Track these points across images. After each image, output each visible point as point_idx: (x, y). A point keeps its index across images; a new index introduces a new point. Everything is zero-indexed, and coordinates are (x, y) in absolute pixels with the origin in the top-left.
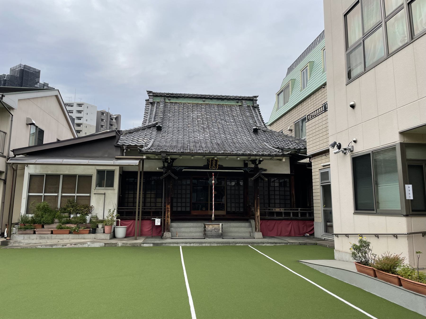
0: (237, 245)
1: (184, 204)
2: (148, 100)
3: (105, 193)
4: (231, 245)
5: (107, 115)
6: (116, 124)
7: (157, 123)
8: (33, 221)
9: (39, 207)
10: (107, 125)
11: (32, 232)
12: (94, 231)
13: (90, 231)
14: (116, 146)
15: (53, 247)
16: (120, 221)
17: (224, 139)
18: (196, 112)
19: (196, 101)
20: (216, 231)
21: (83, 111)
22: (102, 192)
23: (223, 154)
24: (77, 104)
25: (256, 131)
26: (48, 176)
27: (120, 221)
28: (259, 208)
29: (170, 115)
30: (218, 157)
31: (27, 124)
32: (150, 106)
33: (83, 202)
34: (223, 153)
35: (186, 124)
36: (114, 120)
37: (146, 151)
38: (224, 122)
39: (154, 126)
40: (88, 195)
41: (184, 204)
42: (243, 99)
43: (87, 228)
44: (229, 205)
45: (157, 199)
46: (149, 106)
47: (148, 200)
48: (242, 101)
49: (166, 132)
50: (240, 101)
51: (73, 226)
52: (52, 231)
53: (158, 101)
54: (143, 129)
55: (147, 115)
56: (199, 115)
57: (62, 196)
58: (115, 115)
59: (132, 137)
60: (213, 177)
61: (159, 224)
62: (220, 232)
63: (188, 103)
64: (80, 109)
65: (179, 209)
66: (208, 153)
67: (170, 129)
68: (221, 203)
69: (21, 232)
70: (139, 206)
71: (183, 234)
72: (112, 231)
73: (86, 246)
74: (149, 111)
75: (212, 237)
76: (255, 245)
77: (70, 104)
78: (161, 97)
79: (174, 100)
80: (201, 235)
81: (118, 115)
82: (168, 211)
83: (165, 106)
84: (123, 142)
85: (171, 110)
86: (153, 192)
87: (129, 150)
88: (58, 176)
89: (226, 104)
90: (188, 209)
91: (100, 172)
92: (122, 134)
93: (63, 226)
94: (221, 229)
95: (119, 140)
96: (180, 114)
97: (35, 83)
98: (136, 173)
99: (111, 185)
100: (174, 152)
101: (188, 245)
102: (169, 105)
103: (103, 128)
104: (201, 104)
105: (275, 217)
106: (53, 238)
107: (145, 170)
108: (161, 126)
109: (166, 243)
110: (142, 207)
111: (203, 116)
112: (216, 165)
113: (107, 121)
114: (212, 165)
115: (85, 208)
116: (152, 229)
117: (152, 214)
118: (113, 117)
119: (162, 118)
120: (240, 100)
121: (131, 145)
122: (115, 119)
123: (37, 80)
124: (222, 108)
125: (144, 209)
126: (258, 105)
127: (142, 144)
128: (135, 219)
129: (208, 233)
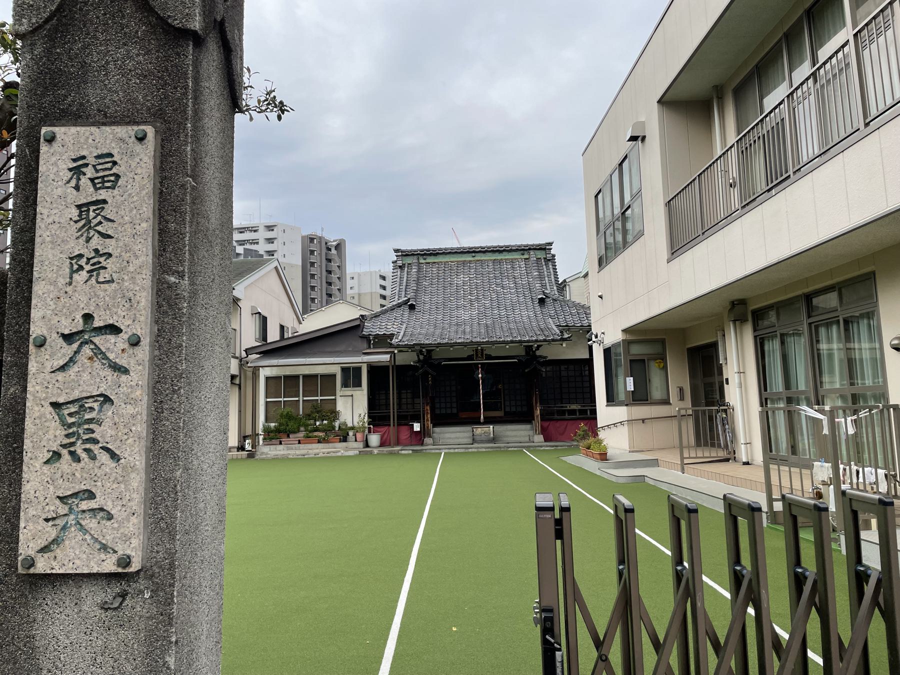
0: (510, 449)
1: (449, 405)
2: (396, 262)
4: (502, 449)
5: (320, 242)
6: (337, 258)
7: (409, 300)
8: (277, 431)
9: (282, 414)
11: (278, 442)
12: (345, 439)
13: (340, 439)
15: (305, 457)
17: (497, 317)
18: (462, 276)
21: (276, 238)
22: (349, 393)
23: (487, 343)
24: (266, 226)
25: (542, 301)
26: (286, 377)
28: (538, 405)
29: (427, 284)
30: (482, 346)
31: (252, 314)
32: (399, 270)
33: (328, 407)
34: (488, 341)
35: (447, 296)
36: (334, 251)
37: (397, 345)
38: (500, 289)
39: (405, 303)
40: (333, 397)
41: (449, 405)
42: (530, 249)
43: (337, 436)
44: (507, 403)
45: (415, 400)
47: (404, 401)
50: (526, 252)
51: (321, 434)
52: (299, 441)
55: (396, 285)
56: (466, 279)
57: (303, 400)
58: (334, 241)
59: (379, 323)
61: (419, 429)
62: (492, 436)
63: (451, 262)
64: (270, 235)
65: (443, 411)
66: (470, 342)
67: (427, 307)
68: (864, 410)
69: (266, 443)
70: (393, 409)
71: (448, 441)
72: (365, 439)
73: (339, 454)
74: (398, 280)
75: (482, 442)
76: (532, 448)
77: (252, 227)
78: (412, 257)
79: (430, 259)
80: (470, 441)
82: (427, 413)
83: (419, 270)
84: (369, 330)
85: (427, 275)
86: (409, 391)
87: (377, 340)
89: (506, 258)
90: (455, 411)
94: (492, 433)
95: (363, 328)
96: (432, 310)
98: (388, 366)
99: (358, 384)
100: (429, 344)
101: (452, 451)
104: (470, 262)
105: (567, 416)
106: (301, 448)
107: (397, 364)
108: (414, 303)
109: (426, 450)
111: (472, 282)
113: (320, 254)
114: (477, 355)
115: (331, 414)
117: (409, 418)
119: (415, 291)
120: (526, 250)
121: (379, 335)
122: (335, 249)
124: (499, 266)
125: (400, 412)
126: (554, 256)
127: (391, 332)
128: (390, 425)
129: (477, 438)
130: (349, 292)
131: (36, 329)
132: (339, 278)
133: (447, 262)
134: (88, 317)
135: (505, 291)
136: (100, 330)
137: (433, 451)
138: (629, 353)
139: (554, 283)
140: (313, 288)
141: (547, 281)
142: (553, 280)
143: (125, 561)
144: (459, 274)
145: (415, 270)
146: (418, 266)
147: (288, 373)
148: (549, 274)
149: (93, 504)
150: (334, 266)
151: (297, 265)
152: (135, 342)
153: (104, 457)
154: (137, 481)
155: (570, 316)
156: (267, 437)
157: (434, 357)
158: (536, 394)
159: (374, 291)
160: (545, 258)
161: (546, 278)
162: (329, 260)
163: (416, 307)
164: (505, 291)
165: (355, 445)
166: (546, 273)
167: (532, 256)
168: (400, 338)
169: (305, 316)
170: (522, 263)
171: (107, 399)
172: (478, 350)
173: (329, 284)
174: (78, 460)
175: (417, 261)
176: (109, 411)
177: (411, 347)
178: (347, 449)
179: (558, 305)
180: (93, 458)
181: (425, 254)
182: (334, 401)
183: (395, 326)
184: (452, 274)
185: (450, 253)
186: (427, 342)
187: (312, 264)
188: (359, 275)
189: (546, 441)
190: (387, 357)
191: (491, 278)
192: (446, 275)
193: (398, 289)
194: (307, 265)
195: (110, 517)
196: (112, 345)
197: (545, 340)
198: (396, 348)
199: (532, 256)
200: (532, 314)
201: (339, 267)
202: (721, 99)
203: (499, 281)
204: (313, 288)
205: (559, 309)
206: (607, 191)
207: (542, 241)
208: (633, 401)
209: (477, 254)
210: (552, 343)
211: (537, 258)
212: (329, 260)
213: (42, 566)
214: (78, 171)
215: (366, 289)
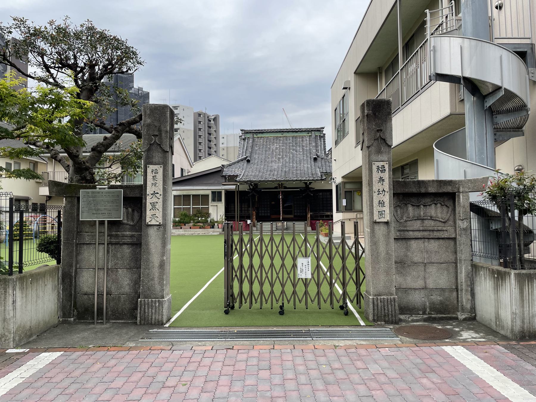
5: (204, 116)
6: (214, 126)
7: (247, 157)
8: (180, 222)
9: (182, 214)
10: (205, 128)
11: (180, 228)
12: (213, 227)
14: (222, 176)
18: (276, 144)
22: (216, 204)
25: (315, 159)
26: (184, 196)
28: (309, 212)
33: (205, 211)
34: (284, 180)
36: (212, 122)
39: (245, 159)
40: (208, 206)
44: (296, 211)
50: (310, 132)
51: (201, 224)
52: (190, 227)
54: (238, 162)
56: (278, 146)
58: (213, 116)
62: (286, 227)
65: (263, 214)
66: (275, 180)
69: (174, 228)
74: (242, 146)
79: (259, 135)
81: (216, 115)
85: (257, 144)
88: (190, 195)
89: (300, 135)
90: (269, 214)
91: (213, 193)
93: (196, 224)
97: (130, 89)
98: (235, 191)
100: (255, 181)
104: (280, 137)
105: (325, 218)
106: (191, 231)
107: (240, 190)
112: (282, 186)
113: (204, 123)
116: (246, 227)
123: (131, 84)
125: (241, 214)
126: (324, 134)
127: (237, 174)
128: (235, 221)
130: (221, 146)
131: (148, 193)
132: (215, 138)
133: (268, 137)
134: (154, 192)
135: (297, 153)
136: (156, 193)
137: (256, 234)
139: (323, 149)
140: (200, 143)
142: (323, 148)
143: (160, 223)
144: (274, 144)
146: (253, 139)
147: (185, 194)
148: (321, 144)
149: (156, 216)
150: (212, 130)
151: (191, 130)
152: (161, 195)
153: (157, 210)
154: (161, 213)
156: (174, 225)
157: (259, 187)
159: (235, 146)
160: (320, 136)
161: (319, 147)
162: (210, 127)
164: (297, 153)
165: (218, 230)
166: (319, 144)
167: (313, 134)
168: (241, 177)
169: (194, 163)
171: (157, 202)
172: (280, 184)
175: (252, 136)
176: (157, 204)
177: (246, 182)
178: (214, 232)
179: (323, 161)
180: (155, 210)
181: (257, 133)
182: (208, 208)
183: (239, 171)
184: (271, 144)
185: (270, 132)
186: (254, 180)
187: (200, 129)
188: (227, 136)
189: (312, 230)
190: (234, 187)
191: (290, 146)
192: (267, 144)
194: (197, 130)
195: (158, 218)
197: (313, 180)
198: (238, 182)
199: (313, 134)
200: (309, 166)
201: (215, 131)
202: (381, 73)
204: (200, 143)
205: (323, 163)
206: (338, 109)
207: (319, 126)
209: (284, 133)
211: (315, 136)
212: (210, 127)
213: (149, 223)
214: (152, 171)
215: (231, 145)
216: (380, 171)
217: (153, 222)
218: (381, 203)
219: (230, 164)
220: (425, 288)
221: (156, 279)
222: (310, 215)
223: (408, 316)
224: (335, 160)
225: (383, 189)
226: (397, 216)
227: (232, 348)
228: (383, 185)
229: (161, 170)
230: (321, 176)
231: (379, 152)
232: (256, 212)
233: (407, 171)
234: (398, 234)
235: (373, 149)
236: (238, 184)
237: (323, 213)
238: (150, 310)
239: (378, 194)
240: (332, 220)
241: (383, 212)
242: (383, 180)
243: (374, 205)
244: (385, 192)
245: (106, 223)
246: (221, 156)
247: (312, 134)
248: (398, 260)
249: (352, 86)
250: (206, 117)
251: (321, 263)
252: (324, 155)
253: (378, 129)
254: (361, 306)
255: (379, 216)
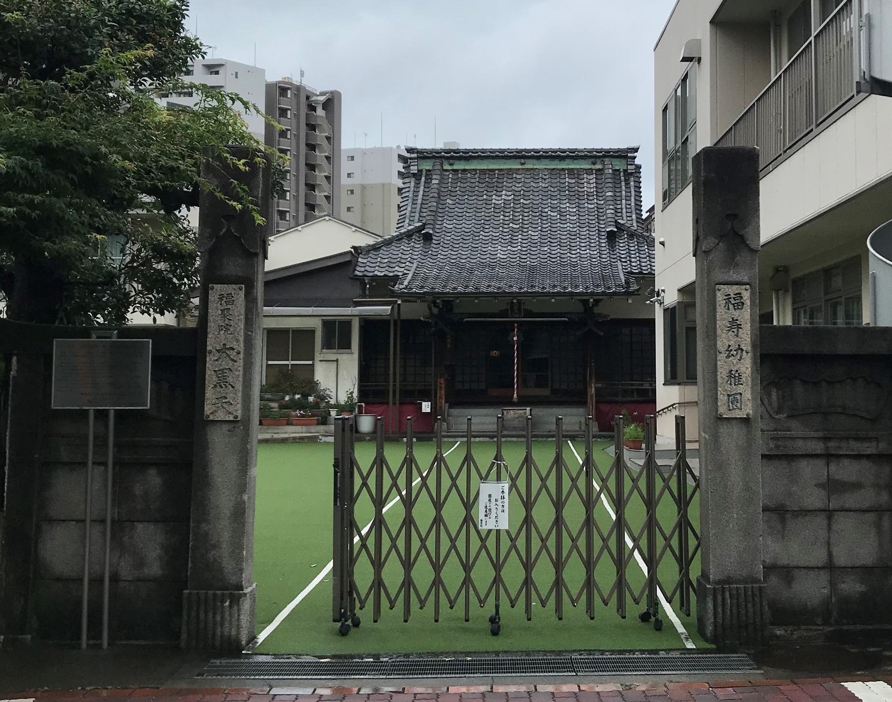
3: (337, 359)
6: (325, 124)
7: (423, 227)
14: (351, 279)
16: (364, 406)
19: (505, 164)
20: (519, 421)
24: (203, 65)
27: (364, 406)
36: (320, 112)
38: (555, 214)
39: (419, 230)
40: (310, 362)
46: (410, 182)
48: (603, 160)
49: (440, 244)
50: (598, 161)
53: (428, 168)
54: (399, 238)
55: (406, 203)
60: (516, 330)
61: (429, 410)
70: (395, 381)
79: (459, 166)
81: (332, 93)
82: (441, 387)
91: (329, 325)
92: (361, 253)
98: (389, 321)
102: (451, 176)
103: (286, 138)
107: (403, 317)
108: (431, 232)
110: (400, 382)
112: (519, 310)
113: (297, 116)
114: (512, 311)
118: (316, 102)
121: (377, 276)
126: (639, 167)
128: (388, 403)
130: (344, 181)
131: (209, 348)
138: (686, 318)
141: (624, 206)
142: (633, 204)
143: (236, 417)
145: (437, 182)
149: (226, 400)
150: (320, 136)
154: (240, 394)
155: (648, 258)
157: (456, 310)
158: (591, 365)
160: (625, 171)
162: (312, 127)
163: (434, 238)
168: (406, 283)
170: (591, 177)
173: (311, 167)
174: (222, 387)
175: (439, 167)
180: (226, 387)
181: (452, 158)
193: (409, 209)
195: (232, 404)
196: (233, 354)
197: (604, 293)
202: (778, 26)
203: (556, 202)
208: (687, 379)
210: (615, 297)
213: (211, 418)
214: (221, 299)
216: (731, 307)
217: (221, 416)
218: (734, 377)
219: (378, 243)
220: (830, 566)
221: (224, 546)
222: (596, 388)
223: (790, 628)
224: (662, 243)
225: (739, 345)
226: (770, 404)
227: (401, 690)
228: (737, 336)
229: (242, 294)
230: (627, 282)
231: (731, 262)
232: (446, 380)
233: (837, 282)
234: (772, 445)
235: (716, 256)
236: (399, 302)
237: (632, 385)
238: (211, 615)
239: (728, 357)
240: (654, 402)
241: (738, 397)
242: (739, 327)
243: (720, 381)
244: (742, 353)
245: (112, 415)
246: (344, 215)
247: (604, 165)
248: (771, 505)
249: (706, 54)
250: (303, 99)
251: (614, 517)
252: (635, 224)
253: (729, 212)
254: (689, 610)
255: (729, 406)
